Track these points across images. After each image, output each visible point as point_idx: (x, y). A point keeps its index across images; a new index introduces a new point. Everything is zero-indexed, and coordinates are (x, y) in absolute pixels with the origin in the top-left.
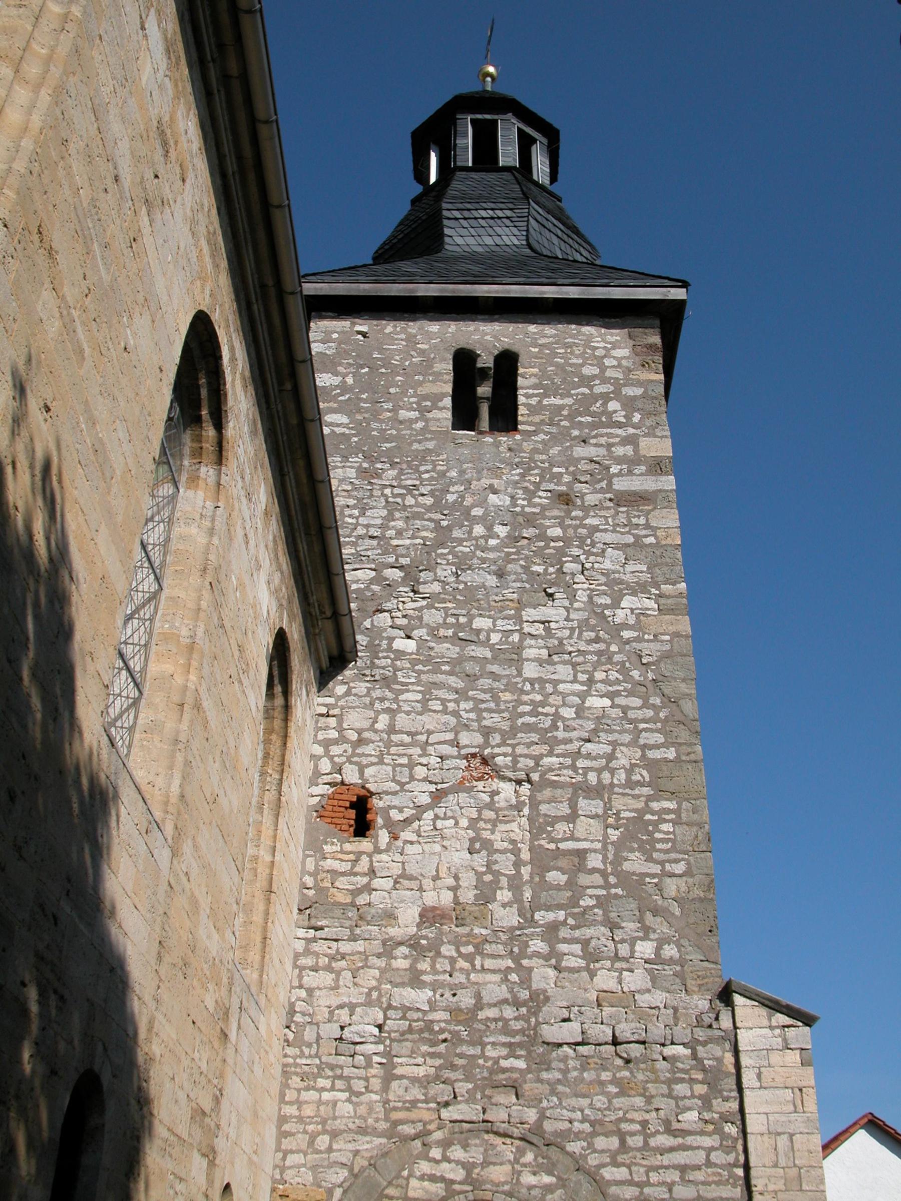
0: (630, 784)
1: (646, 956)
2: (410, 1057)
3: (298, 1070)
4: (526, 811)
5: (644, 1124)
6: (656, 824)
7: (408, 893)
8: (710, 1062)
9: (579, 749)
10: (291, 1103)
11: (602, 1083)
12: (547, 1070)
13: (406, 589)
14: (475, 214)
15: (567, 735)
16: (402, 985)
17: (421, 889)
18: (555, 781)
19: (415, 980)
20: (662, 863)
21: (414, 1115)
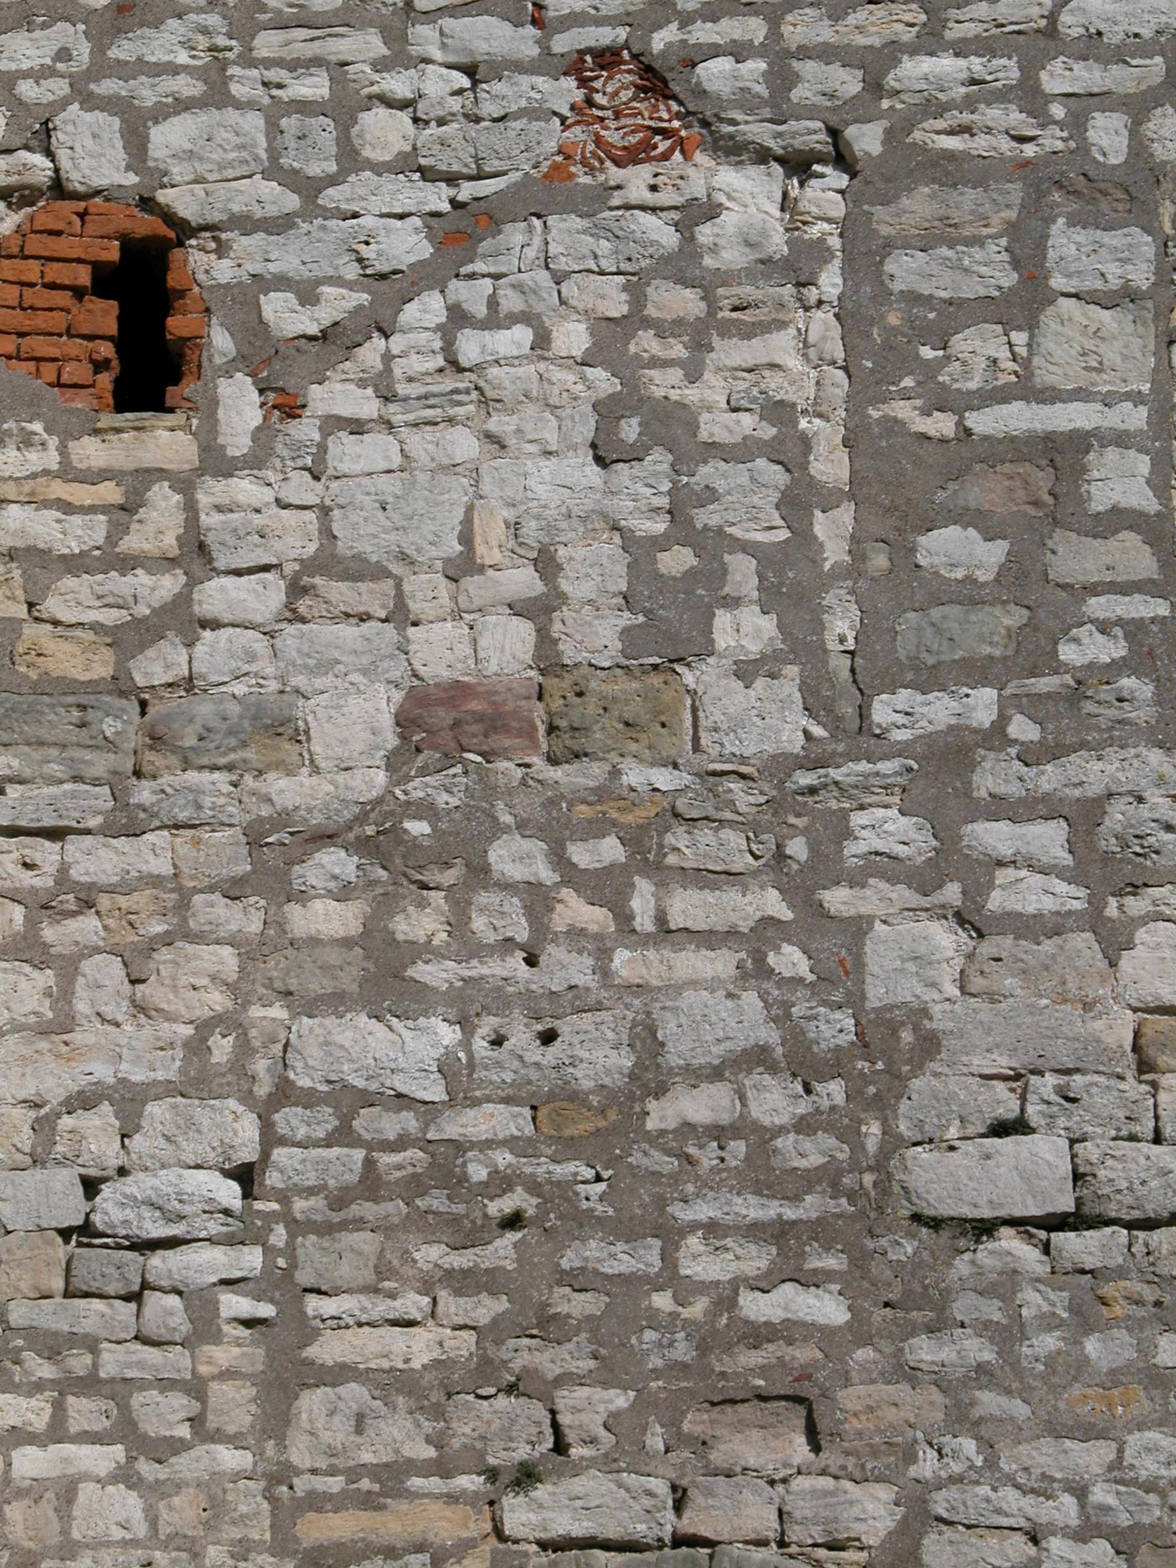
2: (374, 1290)
4: (831, 282)
7: (348, 632)
18: (951, 156)
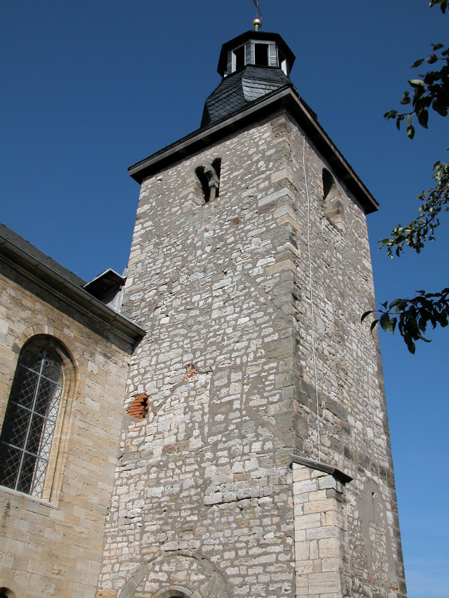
0: (256, 359)
1: (257, 450)
2: (151, 521)
3: (110, 534)
4: (209, 387)
5: (247, 542)
6: (266, 377)
7: (158, 440)
8: (281, 504)
9: (233, 348)
10: (107, 550)
11: (229, 523)
12: (206, 519)
13: (167, 294)
14: (221, 98)
15: (228, 342)
16: (153, 486)
17: (164, 438)
18: (222, 368)
19: (158, 483)
20: (267, 398)
21: (150, 550)
